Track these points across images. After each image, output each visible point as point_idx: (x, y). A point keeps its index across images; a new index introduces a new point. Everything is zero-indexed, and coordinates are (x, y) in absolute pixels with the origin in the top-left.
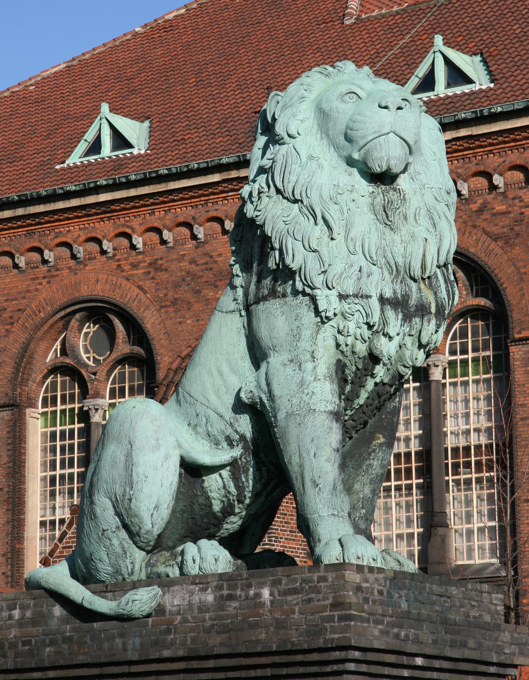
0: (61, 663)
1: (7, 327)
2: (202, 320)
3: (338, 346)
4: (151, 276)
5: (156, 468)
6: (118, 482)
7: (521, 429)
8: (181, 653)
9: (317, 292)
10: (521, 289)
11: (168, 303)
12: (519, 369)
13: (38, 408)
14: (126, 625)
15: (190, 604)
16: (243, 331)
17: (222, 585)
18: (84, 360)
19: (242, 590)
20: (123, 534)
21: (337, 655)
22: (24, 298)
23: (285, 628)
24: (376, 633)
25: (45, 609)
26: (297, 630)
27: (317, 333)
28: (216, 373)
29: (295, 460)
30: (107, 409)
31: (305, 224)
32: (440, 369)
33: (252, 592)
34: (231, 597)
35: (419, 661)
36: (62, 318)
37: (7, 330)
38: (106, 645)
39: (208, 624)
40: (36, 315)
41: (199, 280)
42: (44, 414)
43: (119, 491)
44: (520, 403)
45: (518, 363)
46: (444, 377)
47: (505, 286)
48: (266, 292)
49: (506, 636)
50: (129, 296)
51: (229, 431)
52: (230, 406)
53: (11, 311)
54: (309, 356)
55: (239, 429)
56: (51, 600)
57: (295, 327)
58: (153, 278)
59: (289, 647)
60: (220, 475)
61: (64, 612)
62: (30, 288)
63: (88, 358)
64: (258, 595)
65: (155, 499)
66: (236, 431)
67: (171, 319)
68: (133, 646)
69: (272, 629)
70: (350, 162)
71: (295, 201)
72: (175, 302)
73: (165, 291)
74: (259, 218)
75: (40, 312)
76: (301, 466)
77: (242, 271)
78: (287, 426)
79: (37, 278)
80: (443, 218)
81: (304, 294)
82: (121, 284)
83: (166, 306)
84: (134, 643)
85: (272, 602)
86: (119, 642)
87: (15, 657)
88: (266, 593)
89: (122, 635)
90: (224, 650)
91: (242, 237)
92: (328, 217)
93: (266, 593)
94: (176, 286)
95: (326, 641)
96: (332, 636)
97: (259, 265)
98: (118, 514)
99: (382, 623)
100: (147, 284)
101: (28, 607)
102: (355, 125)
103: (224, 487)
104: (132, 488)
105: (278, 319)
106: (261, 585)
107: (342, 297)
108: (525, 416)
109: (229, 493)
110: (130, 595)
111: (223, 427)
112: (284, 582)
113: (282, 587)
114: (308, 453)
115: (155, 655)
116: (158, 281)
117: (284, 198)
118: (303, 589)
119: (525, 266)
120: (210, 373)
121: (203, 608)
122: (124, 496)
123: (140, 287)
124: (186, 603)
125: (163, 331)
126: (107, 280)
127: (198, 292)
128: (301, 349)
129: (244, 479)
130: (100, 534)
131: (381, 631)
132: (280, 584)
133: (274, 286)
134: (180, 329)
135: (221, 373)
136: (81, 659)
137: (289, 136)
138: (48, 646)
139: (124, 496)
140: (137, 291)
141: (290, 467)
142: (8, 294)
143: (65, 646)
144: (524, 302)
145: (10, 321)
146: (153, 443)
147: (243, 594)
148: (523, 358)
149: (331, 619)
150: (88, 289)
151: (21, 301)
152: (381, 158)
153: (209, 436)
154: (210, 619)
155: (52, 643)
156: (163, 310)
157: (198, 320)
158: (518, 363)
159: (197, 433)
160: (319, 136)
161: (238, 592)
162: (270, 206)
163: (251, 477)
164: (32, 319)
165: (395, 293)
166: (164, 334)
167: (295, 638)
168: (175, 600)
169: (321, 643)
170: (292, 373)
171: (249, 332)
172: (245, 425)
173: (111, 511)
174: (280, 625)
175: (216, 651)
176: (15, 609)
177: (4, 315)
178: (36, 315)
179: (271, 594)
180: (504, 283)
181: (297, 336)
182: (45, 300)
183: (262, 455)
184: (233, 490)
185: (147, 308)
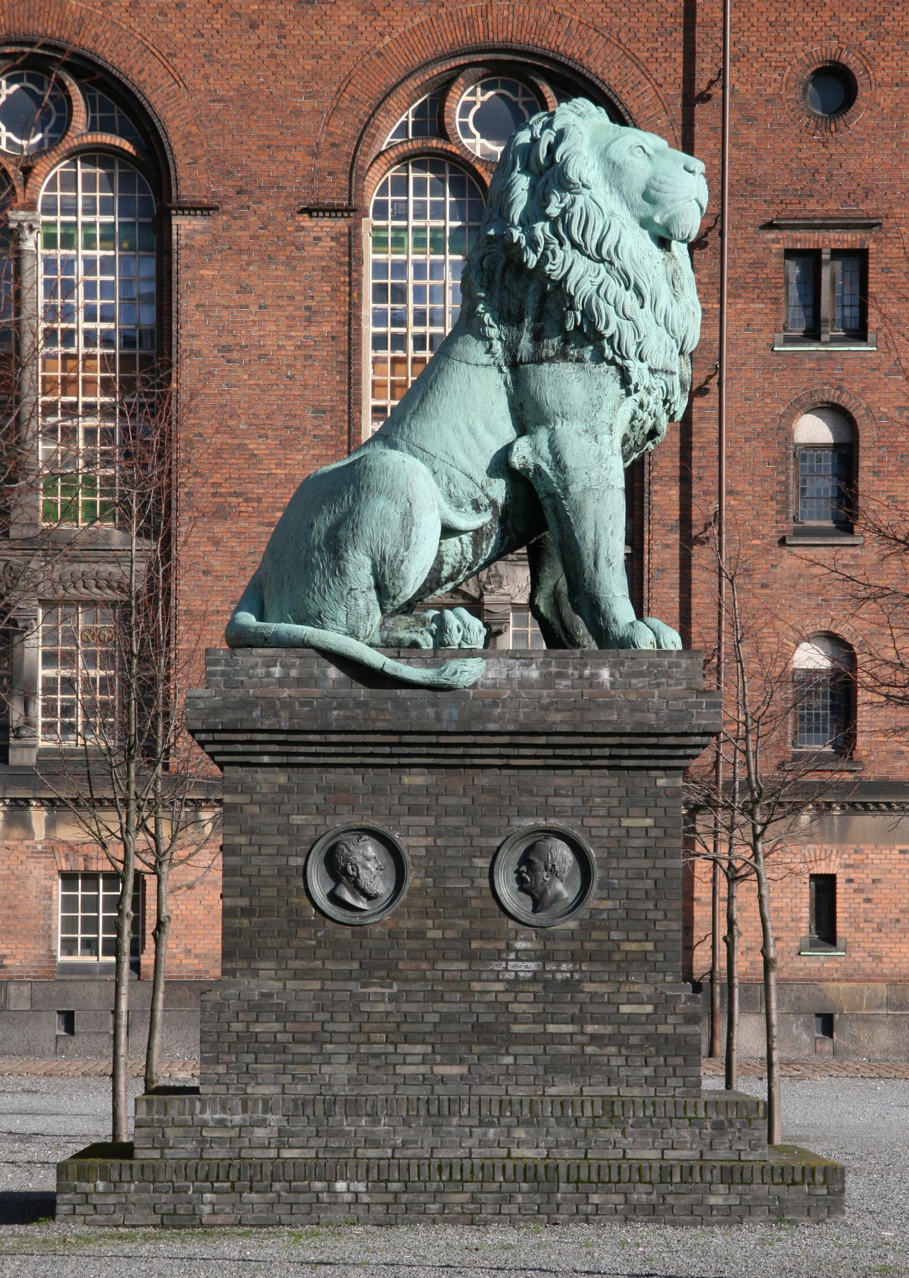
0: (353, 727)
3: (633, 418)
6: (391, 541)
8: (511, 727)
9: (628, 363)
14: (439, 694)
16: (504, 389)
17: (550, 663)
19: (575, 668)
20: (373, 595)
21: (697, 740)
25: (316, 671)
26: (657, 713)
28: (465, 430)
29: (590, 536)
31: (615, 289)
33: (587, 672)
34: (560, 675)
38: (413, 714)
39: (546, 701)
43: (390, 551)
51: (478, 494)
52: (485, 469)
54: (606, 428)
55: (491, 494)
56: (325, 662)
57: (595, 397)
59: (646, 730)
60: (460, 540)
61: (342, 675)
64: (594, 676)
66: (487, 496)
68: (450, 715)
69: (626, 711)
70: (645, 223)
74: (556, 273)
76: (596, 543)
77: (494, 320)
78: (585, 500)
81: (612, 362)
84: (451, 714)
85: (612, 683)
86: (430, 711)
87: (290, 718)
89: (434, 705)
92: (641, 284)
95: (692, 726)
96: (699, 722)
97: (535, 320)
98: (375, 574)
101: (293, 666)
102: (663, 187)
103: (462, 553)
104: (407, 549)
105: (567, 383)
106: (601, 666)
107: (652, 371)
109: (465, 558)
110: (453, 665)
111: (472, 490)
112: (626, 664)
113: (624, 669)
114: (606, 529)
117: (583, 253)
118: (650, 673)
120: (456, 429)
121: (524, 683)
122: (395, 556)
124: (504, 676)
128: (599, 420)
129: (484, 546)
130: (345, 593)
132: (623, 666)
133: (564, 348)
135: (473, 432)
136: (380, 726)
137: (584, 186)
138: (336, 709)
139: (395, 556)
141: (581, 543)
143: (359, 711)
147: (576, 673)
149: (698, 705)
152: (687, 226)
153: (450, 496)
154: (548, 696)
155: (339, 707)
160: (607, 188)
161: (570, 671)
163: (492, 545)
169: (685, 728)
170: (588, 445)
171: (516, 390)
172: (499, 490)
173: (368, 569)
176: (275, 666)
179: (612, 675)
181: (597, 406)
183: (509, 523)
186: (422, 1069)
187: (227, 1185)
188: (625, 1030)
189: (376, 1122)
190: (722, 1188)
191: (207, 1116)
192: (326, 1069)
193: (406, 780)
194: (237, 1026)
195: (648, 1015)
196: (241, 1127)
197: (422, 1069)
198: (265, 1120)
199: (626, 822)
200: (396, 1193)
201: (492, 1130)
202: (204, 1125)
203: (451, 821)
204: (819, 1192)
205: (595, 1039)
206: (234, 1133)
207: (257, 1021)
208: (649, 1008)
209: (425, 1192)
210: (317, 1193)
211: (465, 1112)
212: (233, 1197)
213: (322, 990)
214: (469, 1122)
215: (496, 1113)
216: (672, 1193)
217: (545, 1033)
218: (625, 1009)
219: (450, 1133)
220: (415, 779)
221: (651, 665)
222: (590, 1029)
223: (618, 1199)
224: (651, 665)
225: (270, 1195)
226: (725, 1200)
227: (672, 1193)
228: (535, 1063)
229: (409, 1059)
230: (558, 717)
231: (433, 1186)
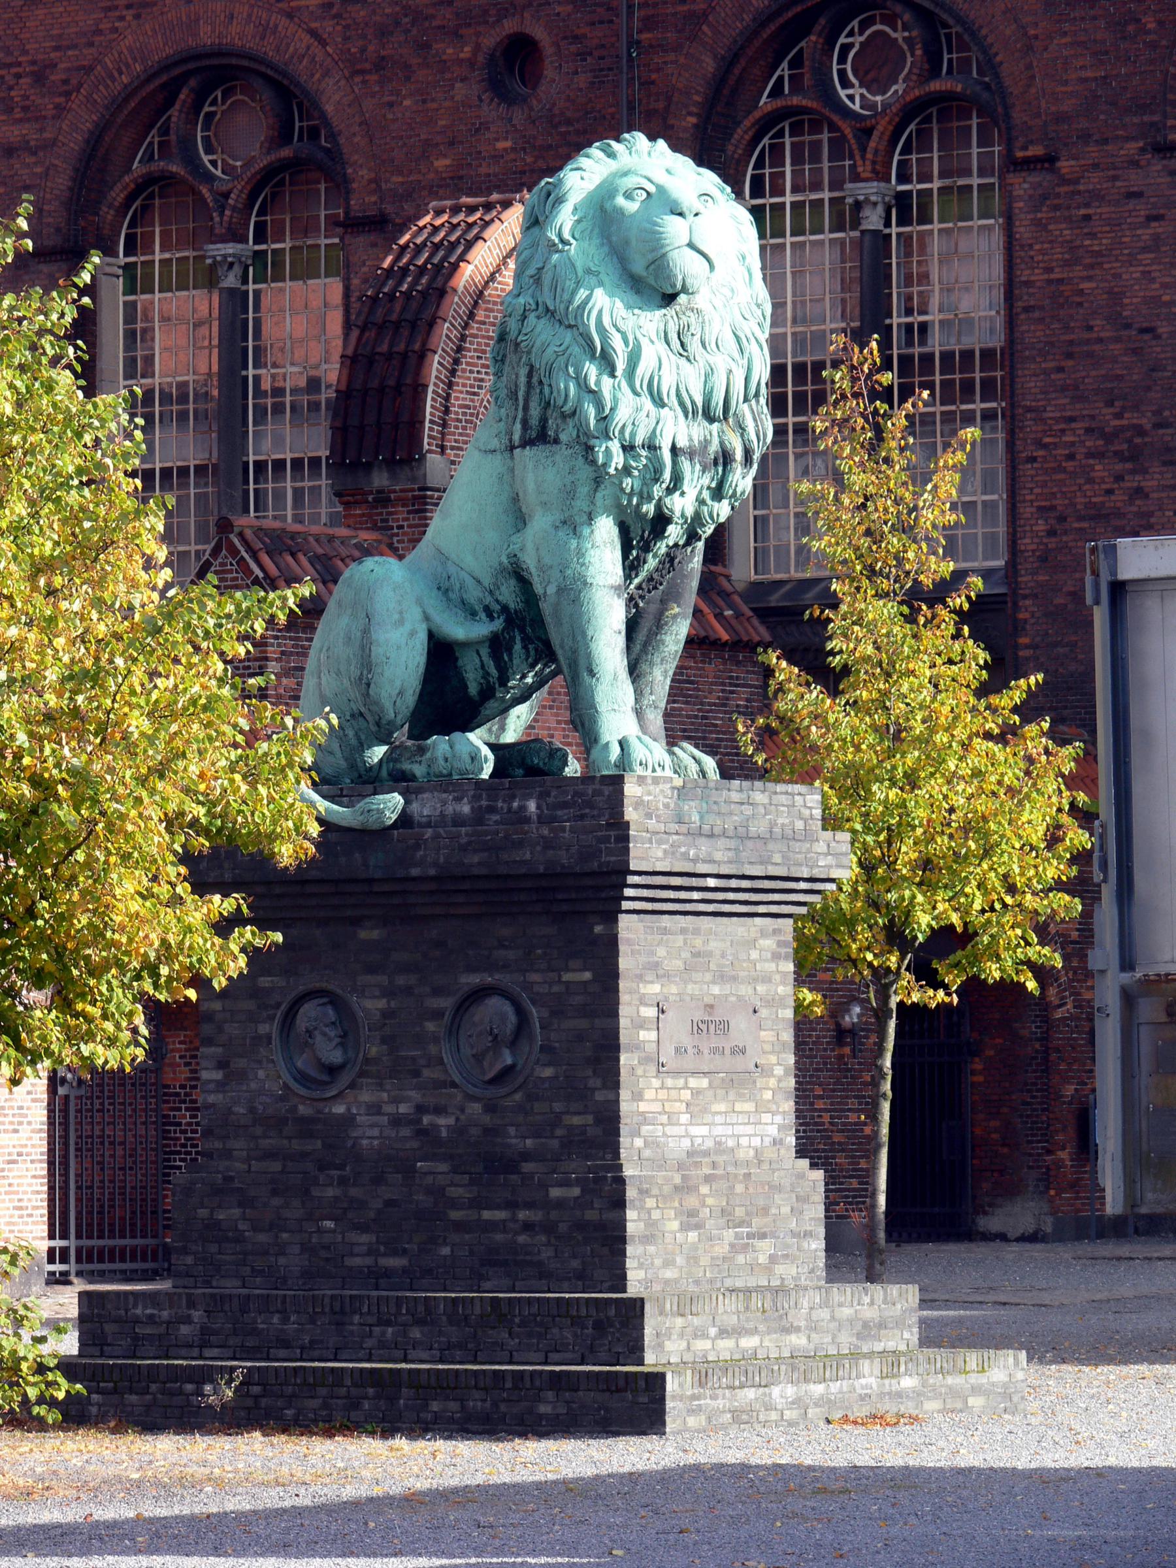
1: (57, 100)
2: (433, 100)
4: (334, 11)
5: (399, 648)
7: (1024, 328)
10: (1029, 66)
11: (367, 66)
12: (1022, 216)
13: (117, 256)
15: (442, 815)
18: (205, 167)
19: (504, 801)
22: (91, 44)
23: (553, 848)
24: (660, 854)
27: (596, 491)
30: (250, 262)
32: (880, 209)
33: (515, 804)
34: (492, 810)
35: (711, 882)
36: (163, 86)
37: (57, 107)
39: (464, 840)
40: (113, 80)
41: (427, 24)
42: (127, 267)
44: (1024, 279)
45: (1021, 204)
46: (888, 224)
47: (998, 59)
48: (534, 434)
49: (821, 847)
50: (291, 49)
51: (488, 600)
53: (68, 69)
58: (338, 16)
62: (102, 26)
63: (214, 163)
64: (523, 808)
65: (398, 683)
66: (497, 601)
67: (373, 97)
69: (539, 848)
71: (570, 326)
72: (380, 64)
73: (361, 43)
75: (121, 73)
79: (116, 7)
80: (753, 341)
82: (276, 26)
83: (362, 72)
85: (539, 817)
88: (532, 806)
90: (484, 871)
91: (504, 356)
93: (532, 806)
94: (383, 32)
99: (667, 842)
100: (327, 27)
104: (370, 671)
108: (1032, 303)
113: (550, 800)
115: (401, 873)
116: (349, 21)
119: (1036, 24)
121: (458, 821)
123: (313, 33)
125: (357, 119)
126: (249, 16)
127: (426, 46)
131: (665, 851)
134: (390, 116)
140: (307, 39)
142: (60, 36)
144: (1033, 90)
145: (65, 88)
146: (396, 616)
148: (1031, 196)
149: (606, 839)
150: (213, 31)
151: (85, 51)
156: (358, 79)
157: (424, 101)
158: (1021, 204)
159: (449, 600)
162: (538, 330)
164: (107, 87)
165: (691, 440)
166: (360, 124)
167: (563, 858)
168: (425, 808)
174: (548, 844)
175: (475, 871)
177: (52, 78)
178: (113, 80)
179: (538, 807)
180: (996, 54)
182: (130, 49)
184: (494, 672)
185: (326, 73)
186: (369, 1261)
187: (111, 1385)
188: (554, 1215)
189: (285, 1320)
190: (550, 1395)
191: (139, 1311)
192: (282, 1261)
193: (363, 934)
194: (203, 1213)
195: (576, 1199)
196: (168, 1323)
197: (369, 1261)
198: (189, 1316)
199: (567, 977)
200: (256, 1397)
201: (390, 1330)
202: (137, 1321)
203: (401, 980)
204: (641, 1400)
205: (528, 1227)
206: (162, 1329)
207: (219, 1207)
208: (576, 1191)
209: (282, 1396)
210: (188, 1395)
211: (365, 1309)
212: (115, 1399)
213: (282, 1172)
214: (371, 1320)
215: (393, 1310)
216: (504, 1400)
217: (479, 1220)
218: (555, 1193)
219: (352, 1332)
220: (369, 934)
221: (576, 794)
222: (522, 1215)
223: (453, 1406)
224: (576, 794)
225: (148, 1397)
226: (554, 1408)
227: (504, 1400)
228: (472, 1253)
229: (356, 1250)
230: (476, 859)
231: (289, 1390)
